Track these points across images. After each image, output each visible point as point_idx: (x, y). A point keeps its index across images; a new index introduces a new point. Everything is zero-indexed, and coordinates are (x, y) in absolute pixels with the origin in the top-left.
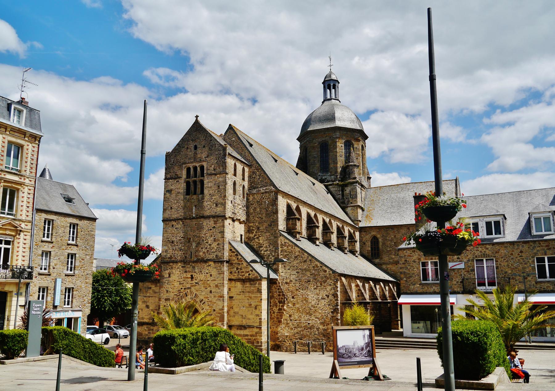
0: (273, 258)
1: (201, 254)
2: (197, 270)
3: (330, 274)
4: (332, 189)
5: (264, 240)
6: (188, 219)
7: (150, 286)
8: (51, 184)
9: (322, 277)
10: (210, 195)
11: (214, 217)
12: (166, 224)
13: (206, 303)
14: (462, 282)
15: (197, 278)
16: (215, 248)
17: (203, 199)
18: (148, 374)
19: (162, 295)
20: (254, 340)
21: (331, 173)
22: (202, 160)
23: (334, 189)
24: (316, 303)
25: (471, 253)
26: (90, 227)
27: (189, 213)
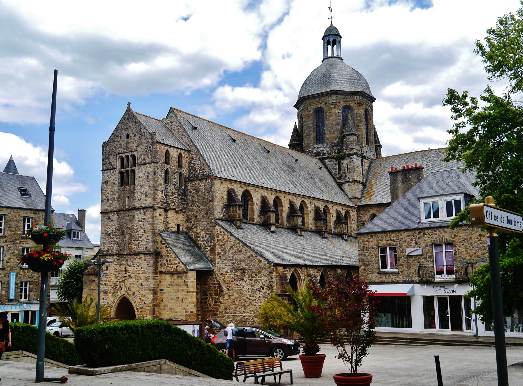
0: (209, 248)
1: (133, 246)
2: (129, 263)
3: (265, 265)
4: (327, 164)
5: (201, 230)
6: (122, 211)
7: (94, 279)
8: (9, 178)
10: (140, 185)
11: (144, 208)
12: (104, 217)
13: (138, 296)
15: (130, 271)
16: (145, 240)
17: (134, 190)
18: (273, 376)
21: (327, 144)
22: (133, 149)
23: (331, 163)
24: (251, 295)
25: (429, 237)
27: (122, 205)
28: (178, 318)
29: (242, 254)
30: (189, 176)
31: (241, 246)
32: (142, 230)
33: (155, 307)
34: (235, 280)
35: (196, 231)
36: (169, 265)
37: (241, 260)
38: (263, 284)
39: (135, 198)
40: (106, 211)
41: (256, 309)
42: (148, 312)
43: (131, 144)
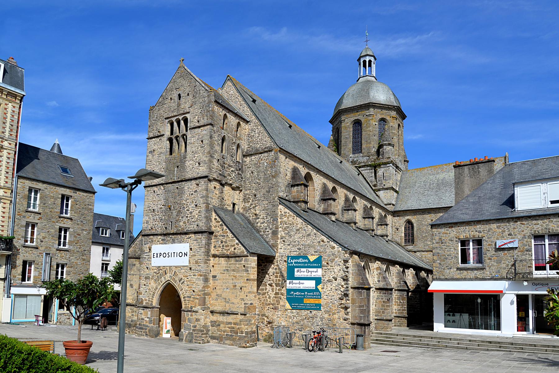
0: (270, 231)
3: (339, 252)
5: (261, 210)
7: (134, 263)
9: (329, 255)
10: (192, 152)
11: (196, 179)
13: (185, 282)
14: (514, 265)
16: (196, 216)
19: (142, 272)
20: (238, 329)
22: (185, 111)
25: (528, 227)
26: (88, 201)
28: (234, 310)
29: (311, 238)
30: (247, 150)
31: (310, 230)
32: (193, 205)
33: (206, 297)
35: (254, 212)
36: (225, 247)
37: (309, 246)
38: (336, 274)
39: (186, 168)
40: (151, 185)
41: (326, 304)
43: (183, 105)
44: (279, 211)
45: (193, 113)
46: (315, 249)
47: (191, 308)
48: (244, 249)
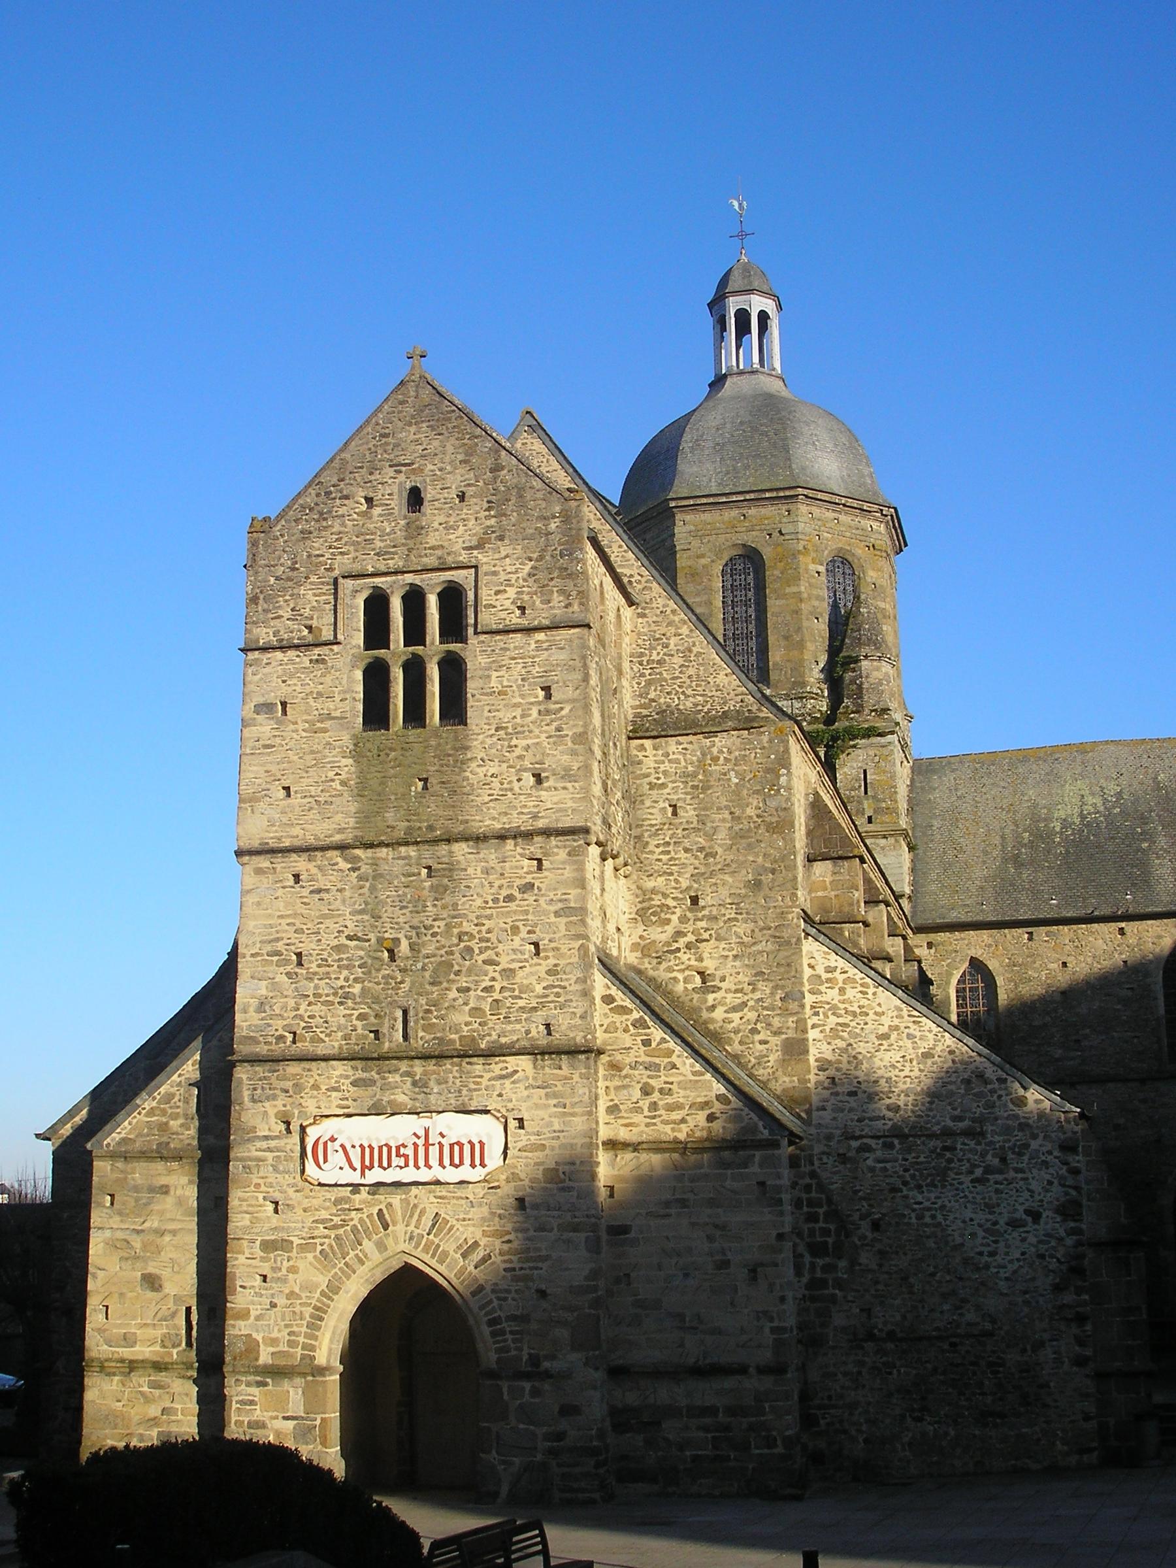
0: (775, 1041)
1: (460, 1017)
7: (164, 1180)
10: (497, 730)
11: (528, 835)
16: (539, 989)
31: (931, 1036)
34: (905, 1183)
38: (1037, 1198)
42: (563, 1334)
44: (805, 961)
45: (495, 573)
46: (954, 1109)
47: (535, 1360)
48: (756, 1118)
